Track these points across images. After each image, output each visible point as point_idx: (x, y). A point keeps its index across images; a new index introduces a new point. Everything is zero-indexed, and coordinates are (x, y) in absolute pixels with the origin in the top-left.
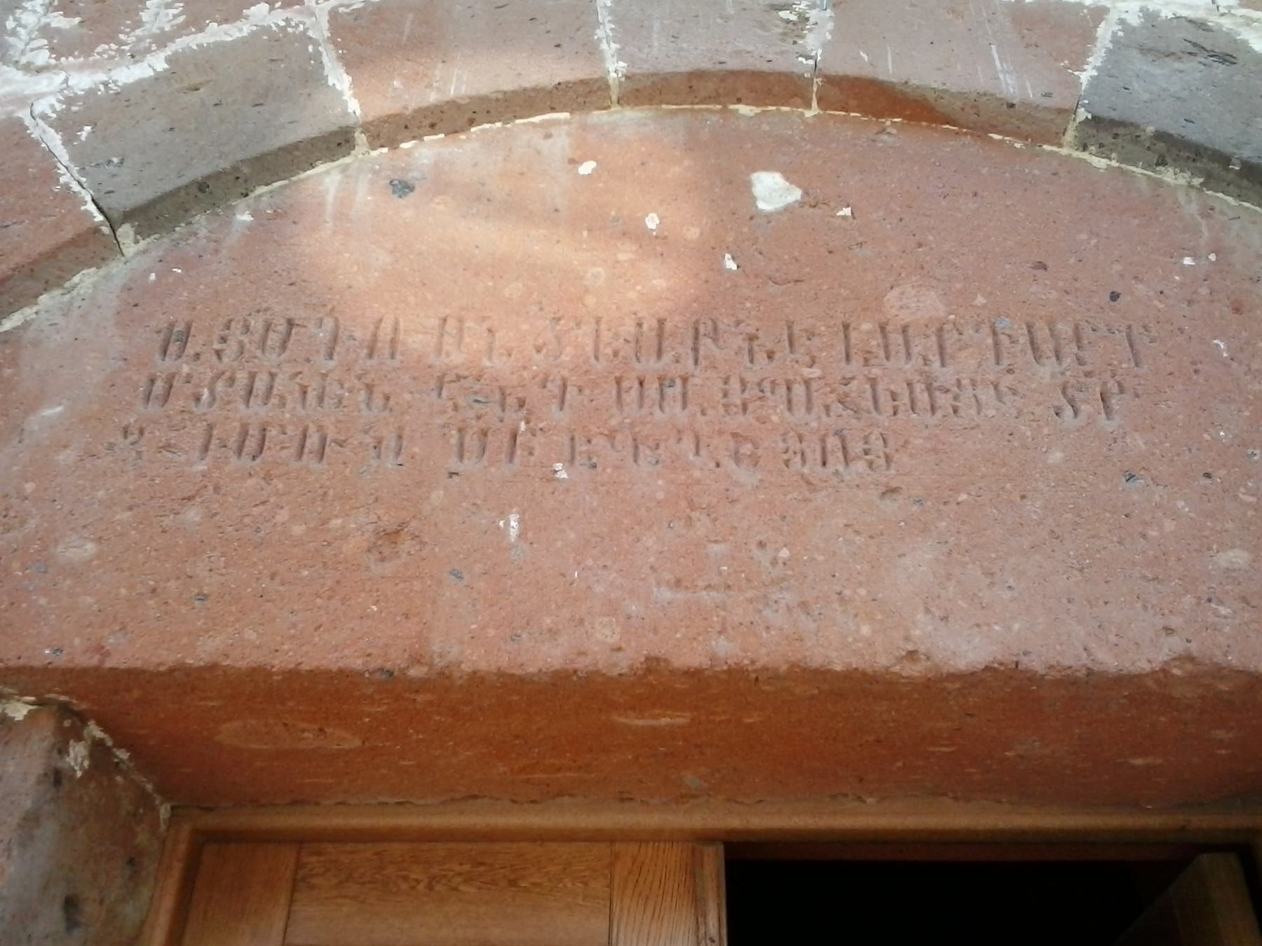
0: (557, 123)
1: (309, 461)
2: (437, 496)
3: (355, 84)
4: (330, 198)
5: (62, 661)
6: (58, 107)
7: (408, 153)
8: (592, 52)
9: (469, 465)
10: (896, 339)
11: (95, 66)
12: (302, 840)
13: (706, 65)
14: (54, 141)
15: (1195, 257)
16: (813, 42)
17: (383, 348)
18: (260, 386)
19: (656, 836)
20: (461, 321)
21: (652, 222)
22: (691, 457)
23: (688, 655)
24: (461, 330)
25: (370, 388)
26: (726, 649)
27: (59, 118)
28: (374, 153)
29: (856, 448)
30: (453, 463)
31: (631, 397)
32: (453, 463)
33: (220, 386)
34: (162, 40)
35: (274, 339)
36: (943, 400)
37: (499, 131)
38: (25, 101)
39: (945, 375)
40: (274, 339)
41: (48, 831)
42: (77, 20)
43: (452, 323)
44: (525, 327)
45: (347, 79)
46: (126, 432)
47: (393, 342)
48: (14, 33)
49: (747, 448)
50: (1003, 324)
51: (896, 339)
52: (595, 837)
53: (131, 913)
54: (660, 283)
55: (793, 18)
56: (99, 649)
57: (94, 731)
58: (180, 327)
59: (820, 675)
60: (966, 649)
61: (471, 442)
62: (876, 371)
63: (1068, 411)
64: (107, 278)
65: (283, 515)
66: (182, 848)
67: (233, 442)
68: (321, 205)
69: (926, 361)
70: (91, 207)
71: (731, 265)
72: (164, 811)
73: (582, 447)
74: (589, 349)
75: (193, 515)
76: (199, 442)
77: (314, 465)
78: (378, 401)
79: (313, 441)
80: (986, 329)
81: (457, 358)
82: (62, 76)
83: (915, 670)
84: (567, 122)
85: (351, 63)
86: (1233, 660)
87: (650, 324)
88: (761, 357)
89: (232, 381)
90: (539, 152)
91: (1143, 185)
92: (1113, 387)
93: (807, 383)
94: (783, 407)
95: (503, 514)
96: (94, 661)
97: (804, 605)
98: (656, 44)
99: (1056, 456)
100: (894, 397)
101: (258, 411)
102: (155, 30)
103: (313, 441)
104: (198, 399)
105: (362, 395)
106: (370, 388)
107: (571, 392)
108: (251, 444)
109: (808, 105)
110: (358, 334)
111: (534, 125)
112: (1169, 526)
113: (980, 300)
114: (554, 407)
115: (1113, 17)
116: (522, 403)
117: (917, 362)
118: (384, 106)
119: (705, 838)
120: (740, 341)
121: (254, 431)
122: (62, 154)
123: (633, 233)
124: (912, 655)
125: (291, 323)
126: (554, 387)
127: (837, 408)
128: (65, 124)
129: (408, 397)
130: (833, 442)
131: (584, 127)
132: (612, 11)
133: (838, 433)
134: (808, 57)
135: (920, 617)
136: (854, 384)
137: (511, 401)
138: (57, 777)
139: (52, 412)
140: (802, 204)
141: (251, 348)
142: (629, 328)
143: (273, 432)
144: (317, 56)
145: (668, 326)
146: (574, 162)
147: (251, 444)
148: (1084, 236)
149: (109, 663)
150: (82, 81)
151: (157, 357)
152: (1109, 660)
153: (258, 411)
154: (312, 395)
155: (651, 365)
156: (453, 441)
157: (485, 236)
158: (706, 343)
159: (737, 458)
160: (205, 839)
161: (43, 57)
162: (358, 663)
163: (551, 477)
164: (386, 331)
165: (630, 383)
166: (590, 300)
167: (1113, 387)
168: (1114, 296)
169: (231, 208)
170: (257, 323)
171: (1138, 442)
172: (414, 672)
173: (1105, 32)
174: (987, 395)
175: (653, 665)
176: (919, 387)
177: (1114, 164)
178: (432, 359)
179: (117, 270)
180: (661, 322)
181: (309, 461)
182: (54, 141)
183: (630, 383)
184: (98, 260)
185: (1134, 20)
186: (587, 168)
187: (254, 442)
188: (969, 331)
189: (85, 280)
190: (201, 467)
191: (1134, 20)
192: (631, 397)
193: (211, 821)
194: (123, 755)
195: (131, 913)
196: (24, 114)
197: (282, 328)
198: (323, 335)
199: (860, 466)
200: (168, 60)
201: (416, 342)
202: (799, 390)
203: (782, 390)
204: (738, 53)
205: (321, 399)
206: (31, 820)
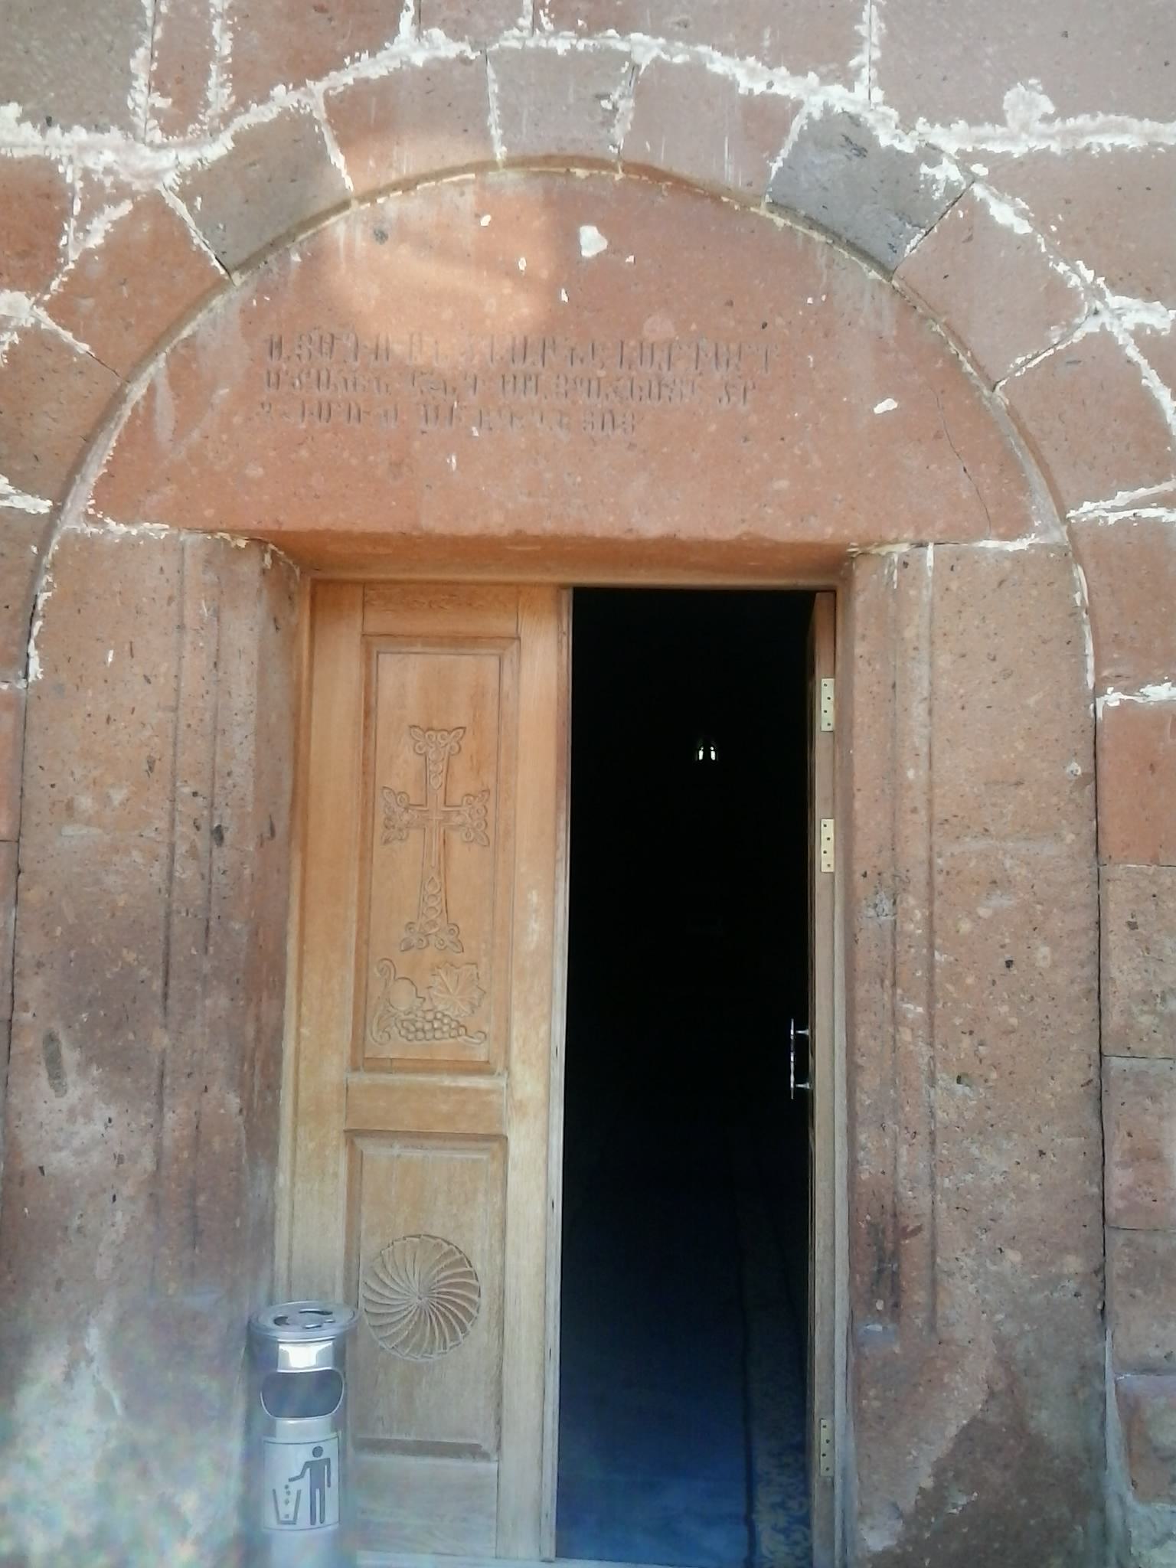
0: (466, 182)
1: (353, 422)
2: (417, 445)
3: (347, 162)
4: (341, 244)
5: (262, 527)
6: (179, 181)
7: (382, 206)
8: (485, 136)
9: (430, 427)
10: (647, 352)
11: (191, 144)
12: (365, 584)
13: (554, 151)
14: (181, 209)
15: (815, 298)
16: (619, 132)
17: (382, 352)
18: (324, 378)
19: (536, 585)
20: (420, 334)
21: (522, 265)
22: (538, 425)
23: (533, 530)
24: (421, 341)
25: (378, 380)
26: (549, 526)
27: (181, 191)
28: (363, 207)
29: (619, 420)
30: (423, 426)
31: (509, 387)
32: (423, 426)
33: (304, 378)
34: (226, 118)
35: (326, 347)
36: (665, 392)
37: (433, 189)
38: (156, 175)
39: (668, 376)
40: (326, 347)
41: (265, 592)
42: (170, 100)
43: (416, 338)
44: (454, 341)
45: (342, 158)
46: (263, 405)
47: (387, 349)
48: (135, 113)
49: (565, 420)
50: (703, 343)
51: (647, 352)
52: (508, 584)
53: (293, 620)
54: (525, 311)
55: (610, 107)
56: (277, 522)
57: (272, 547)
58: (276, 339)
59: (592, 538)
60: (652, 528)
61: (431, 414)
62: (634, 373)
63: (725, 399)
64: (230, 301)
65: (346, 454)
66: (308, 588)
67: (316, 411)
68: (337, 249)
69: (660, 368)
70: (216, 263)
71: (564, 298)
72: (298, 572)
73: (485, 418)
74: (488, 357)
75: (304, 453)
76: (300, 412)
77: (358, 426)
78: (383, 388)
79: (354, 412)
80: (694, 346)
81: (420, 361)
82: (172, 154)
83: (630, 537)
84: (474, 182)
85: (344, 143)
86: (767, 535)
87: (519, 341)
88: (577, 362)
89: (309, 373)
90: (457, 208)
91: (800, 242)
92: (750, 384)
93: (599, 379)
94: (585, 395)
95: (449, 455)
96: (275, 527)
97: (585, 506)
98: (524, 130)
99: (713, 428)
100: (641, 389)
101: (324, 393)
102: (220, 111)
103: (354, 412)
104: (293, 385)
105: (375, 384)
106: (378, 380)
107: (479, 382)
108: (325, 413)
109: (617, 171)
110: (368, 344)
111: (453, 183)
112: (757, 466)
113: (694, 327)
114: (471, 392)
115: (804, 111)
116: (454, 390)
117: (655, 368)
118: (368, 183)
119: (562, 587)
120: (566, 352)
121: (325, 407)
122: (188, 218)
123: (511, 272)
124: (630, 530)
125: (333, 336)
126: (470, 381)
127: (612, 396)
128: (186, 195)
129: (397, 385)
130: (608, 418)
131: (483, 187)
132: (498, 97)
133: (611, 412)
134: (614, 146)
135: (636, 512)
136: (622, 382)
137: (449, 389)
138: (264, 571)
139: (224, 392)
140: (606, 251)
141: (315, 353)
142: (509, 341)
143: (334, 406)
144: (321, 136)
145: (529, 341)
146: (478, 216)
147: (325, 413)
148: (757, 282)
149: (284, 528)
150: (188, 158)
151: (268, 358)
152: (714, 534)
153: (324, 393)
154: (350, 384)
155: (519, 366)
156: (422, 413)
157: (430, 272)
158: (549, 352)
159: (560, 424)
160: (316, 583)
161: (158, 136)
162: (390, 530)
163: (470, 435)
164: (382, 342)
165: (509, 378)
166: (488, 322)
167: (750, 384)
168: (764, 326)
169: (287, 250)
170: (315, 337)
171: (754, 419)
172: (415, 533)
173: (798, 124)
174: (687, 391)
175: (519, 532)
176: (654, 384)
177: (789, 223)
178: (408, 362)
179: (233, 294)
180: (526, 339)
181: (353, 422)
182: (181, 209)
183: (509, 378)
184: (223, 291)
185: (817, 115)
186: (486, 220)
187: (325, 411)
188: (685, 348)
189: (218, 302)
190: (303, 426)
191: (817, 115)
192: (509, 387)
193: (319, 575)
194: (282, 553)
195: (293, 620)
196: (159, 187)
197: (329, 340)
198: (350, 344)
199: (619, 431)
200: (235, 139)
201: (397, 348)
202: (594, 384)
203: (586, 384)
204: (574, 141)
205: (355, 385)
206: (260, 591)
